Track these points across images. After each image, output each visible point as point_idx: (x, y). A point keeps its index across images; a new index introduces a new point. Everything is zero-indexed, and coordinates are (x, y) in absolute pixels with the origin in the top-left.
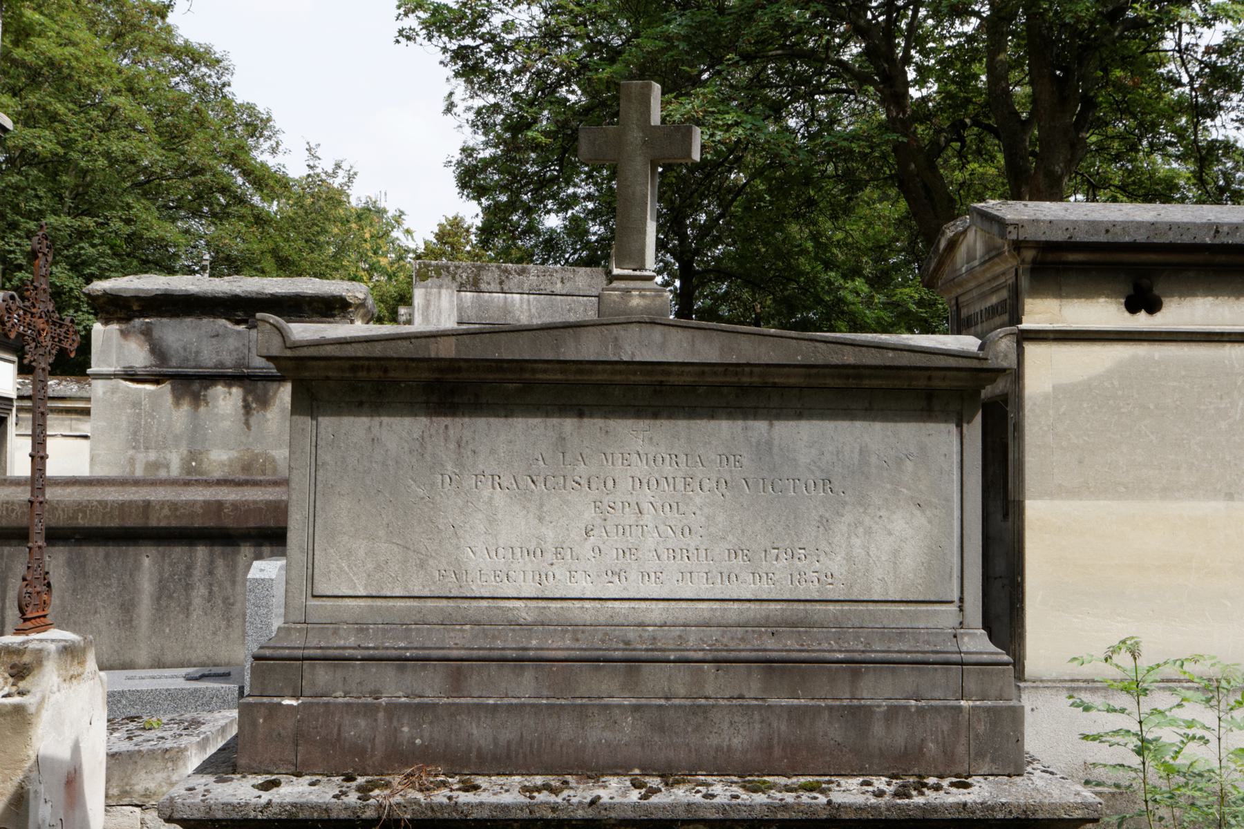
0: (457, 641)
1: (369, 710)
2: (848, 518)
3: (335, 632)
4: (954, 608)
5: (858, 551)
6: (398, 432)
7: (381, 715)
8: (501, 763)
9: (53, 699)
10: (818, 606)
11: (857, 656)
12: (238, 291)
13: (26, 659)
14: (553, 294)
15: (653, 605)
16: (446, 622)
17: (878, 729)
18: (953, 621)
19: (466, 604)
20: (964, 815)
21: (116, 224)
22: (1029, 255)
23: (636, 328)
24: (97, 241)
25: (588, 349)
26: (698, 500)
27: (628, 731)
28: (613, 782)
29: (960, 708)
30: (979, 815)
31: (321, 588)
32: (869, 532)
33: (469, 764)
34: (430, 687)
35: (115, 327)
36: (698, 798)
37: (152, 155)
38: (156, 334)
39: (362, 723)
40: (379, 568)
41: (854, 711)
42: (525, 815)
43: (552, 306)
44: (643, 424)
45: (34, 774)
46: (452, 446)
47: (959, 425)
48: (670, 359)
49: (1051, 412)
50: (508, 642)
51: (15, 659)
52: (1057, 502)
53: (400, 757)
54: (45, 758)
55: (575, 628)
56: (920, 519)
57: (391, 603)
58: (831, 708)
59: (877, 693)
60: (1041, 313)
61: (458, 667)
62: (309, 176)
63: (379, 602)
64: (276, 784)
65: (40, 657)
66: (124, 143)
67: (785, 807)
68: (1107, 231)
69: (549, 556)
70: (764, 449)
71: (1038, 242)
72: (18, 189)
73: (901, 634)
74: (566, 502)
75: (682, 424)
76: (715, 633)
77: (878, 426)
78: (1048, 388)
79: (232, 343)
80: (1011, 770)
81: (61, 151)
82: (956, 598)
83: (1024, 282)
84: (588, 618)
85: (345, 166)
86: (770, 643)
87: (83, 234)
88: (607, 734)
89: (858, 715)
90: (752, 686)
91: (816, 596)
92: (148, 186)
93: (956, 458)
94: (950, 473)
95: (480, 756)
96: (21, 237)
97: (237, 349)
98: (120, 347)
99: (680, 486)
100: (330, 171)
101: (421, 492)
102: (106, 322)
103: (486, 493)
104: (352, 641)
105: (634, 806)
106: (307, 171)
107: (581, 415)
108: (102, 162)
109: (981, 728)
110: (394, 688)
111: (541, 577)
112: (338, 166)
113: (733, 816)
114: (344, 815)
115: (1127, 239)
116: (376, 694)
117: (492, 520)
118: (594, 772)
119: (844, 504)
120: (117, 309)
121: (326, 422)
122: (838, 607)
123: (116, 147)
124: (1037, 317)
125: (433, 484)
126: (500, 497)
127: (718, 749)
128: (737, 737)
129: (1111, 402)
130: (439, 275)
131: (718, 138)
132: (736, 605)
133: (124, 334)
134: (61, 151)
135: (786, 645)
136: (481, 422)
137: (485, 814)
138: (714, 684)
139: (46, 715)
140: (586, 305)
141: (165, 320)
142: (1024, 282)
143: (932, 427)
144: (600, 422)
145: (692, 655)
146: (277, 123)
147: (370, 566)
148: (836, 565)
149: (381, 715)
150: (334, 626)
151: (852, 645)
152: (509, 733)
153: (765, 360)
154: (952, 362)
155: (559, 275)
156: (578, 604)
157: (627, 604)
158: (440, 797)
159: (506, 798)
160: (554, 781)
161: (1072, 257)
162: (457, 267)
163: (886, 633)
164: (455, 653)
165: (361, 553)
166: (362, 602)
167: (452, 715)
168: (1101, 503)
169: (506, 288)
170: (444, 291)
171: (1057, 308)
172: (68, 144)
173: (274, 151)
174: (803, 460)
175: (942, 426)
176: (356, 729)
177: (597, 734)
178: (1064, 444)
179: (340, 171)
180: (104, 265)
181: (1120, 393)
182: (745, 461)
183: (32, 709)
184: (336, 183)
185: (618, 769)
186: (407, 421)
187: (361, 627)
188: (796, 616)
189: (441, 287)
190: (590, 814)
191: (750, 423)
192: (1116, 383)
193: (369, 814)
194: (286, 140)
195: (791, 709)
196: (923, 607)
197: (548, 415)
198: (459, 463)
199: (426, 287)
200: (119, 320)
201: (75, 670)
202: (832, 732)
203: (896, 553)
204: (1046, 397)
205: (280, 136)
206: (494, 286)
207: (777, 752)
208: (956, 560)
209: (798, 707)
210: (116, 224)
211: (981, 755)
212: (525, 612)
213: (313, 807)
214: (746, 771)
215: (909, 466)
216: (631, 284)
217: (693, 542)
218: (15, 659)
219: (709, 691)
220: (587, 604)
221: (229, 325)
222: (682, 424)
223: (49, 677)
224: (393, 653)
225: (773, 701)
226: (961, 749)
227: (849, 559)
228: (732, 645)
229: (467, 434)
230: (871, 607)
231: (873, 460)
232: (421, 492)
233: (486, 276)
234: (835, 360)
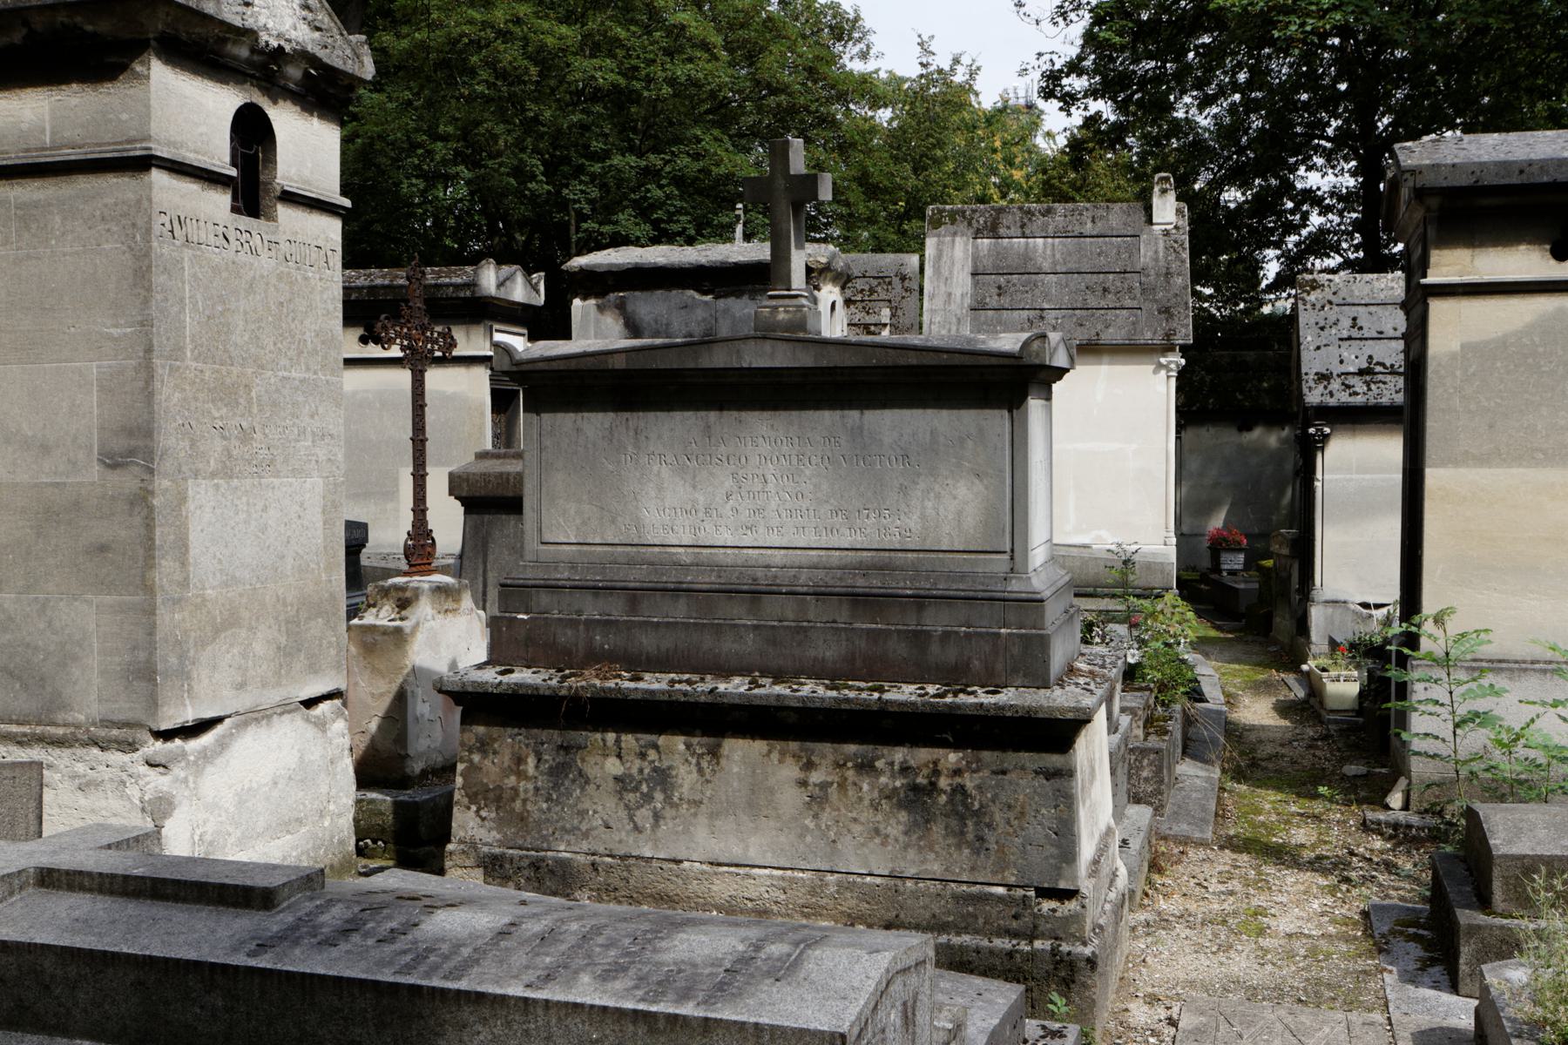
0: (635, 576)
1: (573, 624)
2: (922, 486)
3: (556, 568)
4: (1006, 557)
5: (930, 512)
6: (595, 423)
7: (581, 627)
8: (659, 664)
9: (427, 625)
10: (900, 554)
11: (922, 592)
12: (703, 261)
13: (408, 594)
14: (1081, 236)
15: (776, 552)
16: (631, 563)
17: (935, 648)
18: (1005, 567)
19: (643, 550)
20: (981, 713)
21: (683, 161)
22: (1434, 202)
23: (752, 342)
24: (664, 182)
25: (718, 359)
26: (807, 472)
27: (749, 644)
28: (737, 680)
29: (999, 634)
30: (992, 712)
31: (548, 537)
32: (938, 496)
33: (638, 664)
34: (616, 609)
35: (592, 302)
36: (788, 691)
37: (721, 74)
38: (630, 308)
39: (569, 633)
40: (584, 523)
41: (916, 634)
42: (666, 698)
43: (1080, 250)
44: (767, 414)
45: (411, 679)
46: (632, 433)
47: (1010, 411)
48: (777, 364)
49: (1458, 373)
50: (670, 578)
51: (401, 594)
52: (1462, 470)
53: (594, 657)
54: (421, 669)
55: (719, 567)
56: (979, 486)
57: (593, 548)
58: (899, 631)
59: (936, 621)
60: (1448, 266)
61: (634, 595)
62: (922, 76)
63: (585, 548)
64: (512, 671)
65: (417, 593)
66: (690, 66)
67: (847, 700)
68: (1521, 172)
69: (701, 515)
70: (857, 432)
71: (1442, 188)
72: (584, 127)
73: (963, 576)
74: (711, 474)
75: (794, 414)
76: (821, 574)
77: (945, 413)
78: (1455, 346)
79: (700, 313)
80: (1039, 683)
81: (622, 81)
82: (1008, 548)
83: (1431, 233)
84: (729, 561)
85: (965, 60)
86: (860, 582)
87: (650, 174)
88: (736, 646)
89: (919, 638)
90: (843, 615)
91: (898, 546)
92: (722, 114)
93: (1007, 437)
94: (1003, 449)
95: (649, 659)
96: (586, 184)
97: (704, 320)
98: (597, 321)
99: (795, 462)
100: (947, 68)
101: (611, 467)
102: (584, 298)
103: (656, 468)
104: (566, 575)
105: (741, 695)
106: (919, 70)
107: (721, 409)
108: (666, 90)
109: (1016, 650)
110: (592, 609)
111: (695, 530)
112: (956, 61)
113: (810, 705)
114: (547, 693)
115: (1545, 179)
116: (579, 613)
117: (660, 489)
118: (726, 673)
119: (919, 475)
120: (598, 284)
121: (545, 416)
122: (915, 555)
123: (681, 71)
124: (1445, 270)
125: (619, 462)
126: (665, 472)
127: (815, 659)
128: (829, 651)
129: (1530, 360)
130: (953, 222)
131: (1308, 28)
132: (837, 553)
133: (601, 309)
134: (622, 81)
135: (875, 583)
136: (651, 415)
137: (639, 696)
138: (816, 612)
139: (420, 637)
140: (1119, 247)
141: (637, 293)
142: (1431, 233)
143: (988, 413)
144: (735, 414)
145: (799, 589)
146: (868, 22)
147: (578, 521)
148: (913, 522)
149: (581, 627)
150: (555, 564)
151: (922, 584)
152: (667, 642)
153: (848, 363)
154: (994, 361)
155: (1090, 214)
156: (722, 551)
157: (757, 551)
158: (611, 684)
159: (656, 686)
160: (695, 677)
161: (1486, 202)
162: (974, 211)
163: (951, 576)
164: (632, 585)
165: (572, 512)
166: (574, 548)
167: (629, 629)
168: (1514, 471)
169: (1027, 232)
170: (958, 239)
171: (1468, 259)
172: (631, 73)
173: (864, 56)
174: (887, 440)
175: (996, 412)
176: (565, 637)
177: (728, 646)
178: (1473, 407)
179: (958, 67)
180: (672, 209)
181: (1541, 350)
182: (843, 442)
183: (407, 631)
184: (959, 77)
185: (741, 672)
186: (600, 415)
187: (573, 566)
188: (882, 562)
189: (955, 234)
190: (709, 699)
191: (846, 412)
192: (1537, 339)
193: (563, 692)
194: (878, 42)
195: (869, 631)
196: (982, 556)
197: (697, 409)
198: (637, 446)
199: (938, 236)
200: (597, 296)
201: (450, 605)
202: (899, 650)
203: (959, 513)
204: (1453, 356)
205: (872, 38)
206: (1015, 231)
207: (859, 663)
208: (1008, 518)
209: (874, 630)
210: (683, 161)
211: (1015, 670)
212: (684, 555)
213: (529, 686)
214: (833, 676)
215: (970, 444)
216: (781, 302)
217: (805, 504)
218: (401, 594)
219: (811, 616)
220: (729, 551)
221: (697, 296)
222: (795, 413)
223: (424, 609)
224: (591, 584)
225: (856, 625)
226: (999, 666)
227: (923, 517)
228: (831, 583)
229: (642, 424)
230: (941, 555)
231: (942, 439)
232: (611, 467)
233: (1006, 220)
234: (902, 362)
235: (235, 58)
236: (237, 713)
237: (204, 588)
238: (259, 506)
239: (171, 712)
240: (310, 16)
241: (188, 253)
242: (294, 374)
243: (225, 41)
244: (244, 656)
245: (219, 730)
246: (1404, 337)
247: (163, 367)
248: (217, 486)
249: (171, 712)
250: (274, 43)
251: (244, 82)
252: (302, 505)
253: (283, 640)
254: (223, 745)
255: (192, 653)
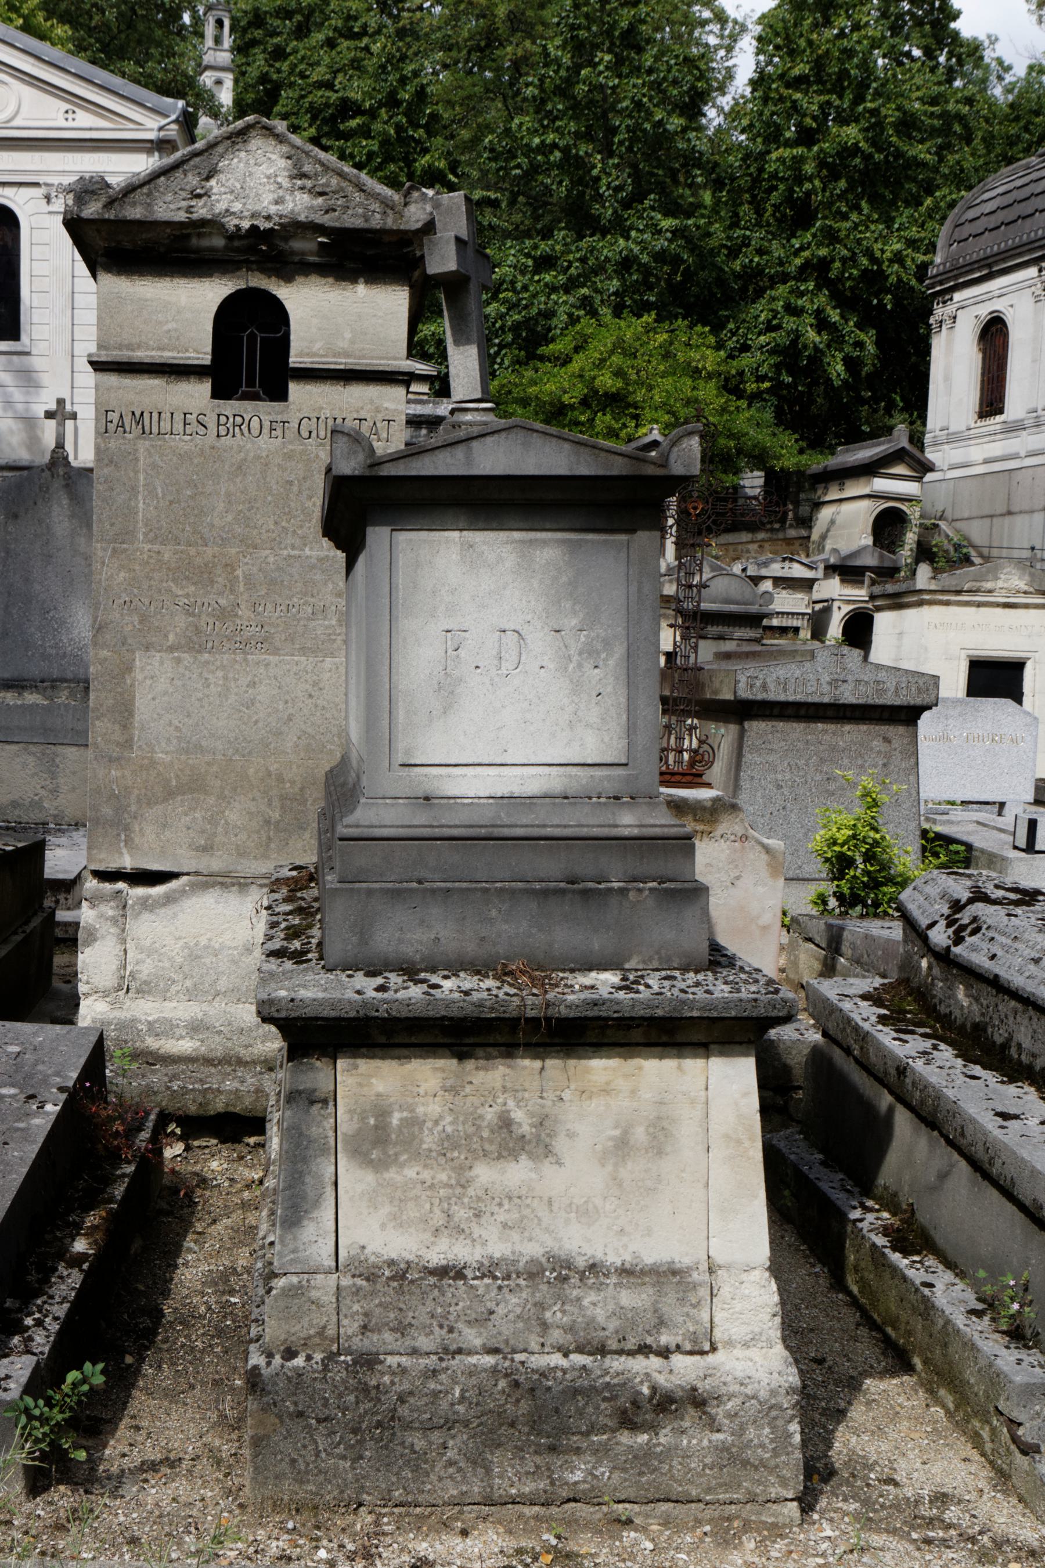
235: (213, 249)
236: (197, 873)
237: (153, 751)
238: (244, 681)
239: (102, 856)
240: (309, 183)
241: (143, 445)
242: (307, 552)
243: (188, 236)
244: (212, 821)
245: (174, 884)
246: (741, 724)
247: (105, 550)
248: (178, 661)
249: (102, 856)
250: (246, 225)
251: (239, 269)
252: (315, 684)
253: (276, 815)
254: (169, 900)
255: (133, 808)
